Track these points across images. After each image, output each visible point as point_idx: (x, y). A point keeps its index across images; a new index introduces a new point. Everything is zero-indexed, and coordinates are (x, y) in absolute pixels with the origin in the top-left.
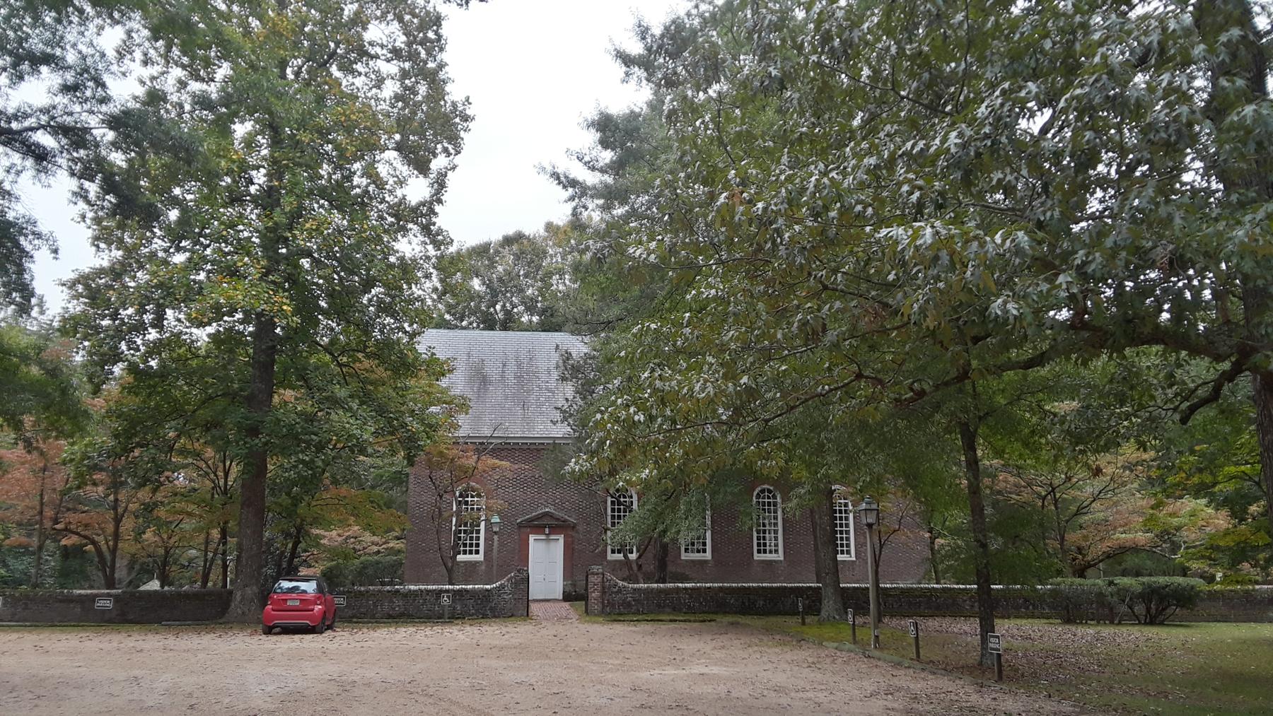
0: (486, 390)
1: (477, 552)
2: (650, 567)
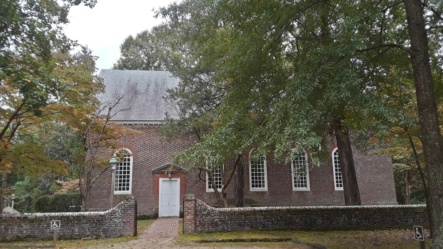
0: (136, 97)
1: (128, 189)
2: (231, 196)
